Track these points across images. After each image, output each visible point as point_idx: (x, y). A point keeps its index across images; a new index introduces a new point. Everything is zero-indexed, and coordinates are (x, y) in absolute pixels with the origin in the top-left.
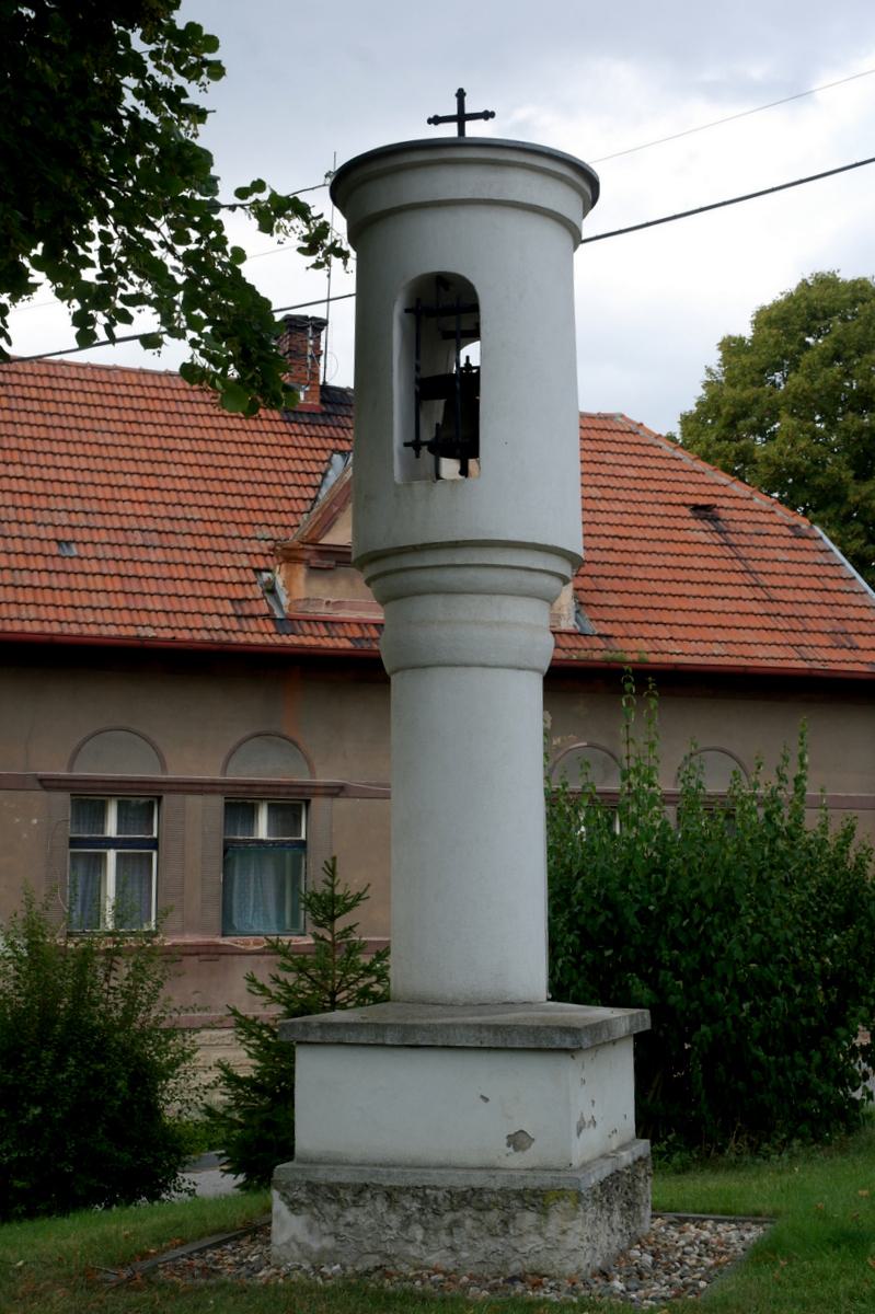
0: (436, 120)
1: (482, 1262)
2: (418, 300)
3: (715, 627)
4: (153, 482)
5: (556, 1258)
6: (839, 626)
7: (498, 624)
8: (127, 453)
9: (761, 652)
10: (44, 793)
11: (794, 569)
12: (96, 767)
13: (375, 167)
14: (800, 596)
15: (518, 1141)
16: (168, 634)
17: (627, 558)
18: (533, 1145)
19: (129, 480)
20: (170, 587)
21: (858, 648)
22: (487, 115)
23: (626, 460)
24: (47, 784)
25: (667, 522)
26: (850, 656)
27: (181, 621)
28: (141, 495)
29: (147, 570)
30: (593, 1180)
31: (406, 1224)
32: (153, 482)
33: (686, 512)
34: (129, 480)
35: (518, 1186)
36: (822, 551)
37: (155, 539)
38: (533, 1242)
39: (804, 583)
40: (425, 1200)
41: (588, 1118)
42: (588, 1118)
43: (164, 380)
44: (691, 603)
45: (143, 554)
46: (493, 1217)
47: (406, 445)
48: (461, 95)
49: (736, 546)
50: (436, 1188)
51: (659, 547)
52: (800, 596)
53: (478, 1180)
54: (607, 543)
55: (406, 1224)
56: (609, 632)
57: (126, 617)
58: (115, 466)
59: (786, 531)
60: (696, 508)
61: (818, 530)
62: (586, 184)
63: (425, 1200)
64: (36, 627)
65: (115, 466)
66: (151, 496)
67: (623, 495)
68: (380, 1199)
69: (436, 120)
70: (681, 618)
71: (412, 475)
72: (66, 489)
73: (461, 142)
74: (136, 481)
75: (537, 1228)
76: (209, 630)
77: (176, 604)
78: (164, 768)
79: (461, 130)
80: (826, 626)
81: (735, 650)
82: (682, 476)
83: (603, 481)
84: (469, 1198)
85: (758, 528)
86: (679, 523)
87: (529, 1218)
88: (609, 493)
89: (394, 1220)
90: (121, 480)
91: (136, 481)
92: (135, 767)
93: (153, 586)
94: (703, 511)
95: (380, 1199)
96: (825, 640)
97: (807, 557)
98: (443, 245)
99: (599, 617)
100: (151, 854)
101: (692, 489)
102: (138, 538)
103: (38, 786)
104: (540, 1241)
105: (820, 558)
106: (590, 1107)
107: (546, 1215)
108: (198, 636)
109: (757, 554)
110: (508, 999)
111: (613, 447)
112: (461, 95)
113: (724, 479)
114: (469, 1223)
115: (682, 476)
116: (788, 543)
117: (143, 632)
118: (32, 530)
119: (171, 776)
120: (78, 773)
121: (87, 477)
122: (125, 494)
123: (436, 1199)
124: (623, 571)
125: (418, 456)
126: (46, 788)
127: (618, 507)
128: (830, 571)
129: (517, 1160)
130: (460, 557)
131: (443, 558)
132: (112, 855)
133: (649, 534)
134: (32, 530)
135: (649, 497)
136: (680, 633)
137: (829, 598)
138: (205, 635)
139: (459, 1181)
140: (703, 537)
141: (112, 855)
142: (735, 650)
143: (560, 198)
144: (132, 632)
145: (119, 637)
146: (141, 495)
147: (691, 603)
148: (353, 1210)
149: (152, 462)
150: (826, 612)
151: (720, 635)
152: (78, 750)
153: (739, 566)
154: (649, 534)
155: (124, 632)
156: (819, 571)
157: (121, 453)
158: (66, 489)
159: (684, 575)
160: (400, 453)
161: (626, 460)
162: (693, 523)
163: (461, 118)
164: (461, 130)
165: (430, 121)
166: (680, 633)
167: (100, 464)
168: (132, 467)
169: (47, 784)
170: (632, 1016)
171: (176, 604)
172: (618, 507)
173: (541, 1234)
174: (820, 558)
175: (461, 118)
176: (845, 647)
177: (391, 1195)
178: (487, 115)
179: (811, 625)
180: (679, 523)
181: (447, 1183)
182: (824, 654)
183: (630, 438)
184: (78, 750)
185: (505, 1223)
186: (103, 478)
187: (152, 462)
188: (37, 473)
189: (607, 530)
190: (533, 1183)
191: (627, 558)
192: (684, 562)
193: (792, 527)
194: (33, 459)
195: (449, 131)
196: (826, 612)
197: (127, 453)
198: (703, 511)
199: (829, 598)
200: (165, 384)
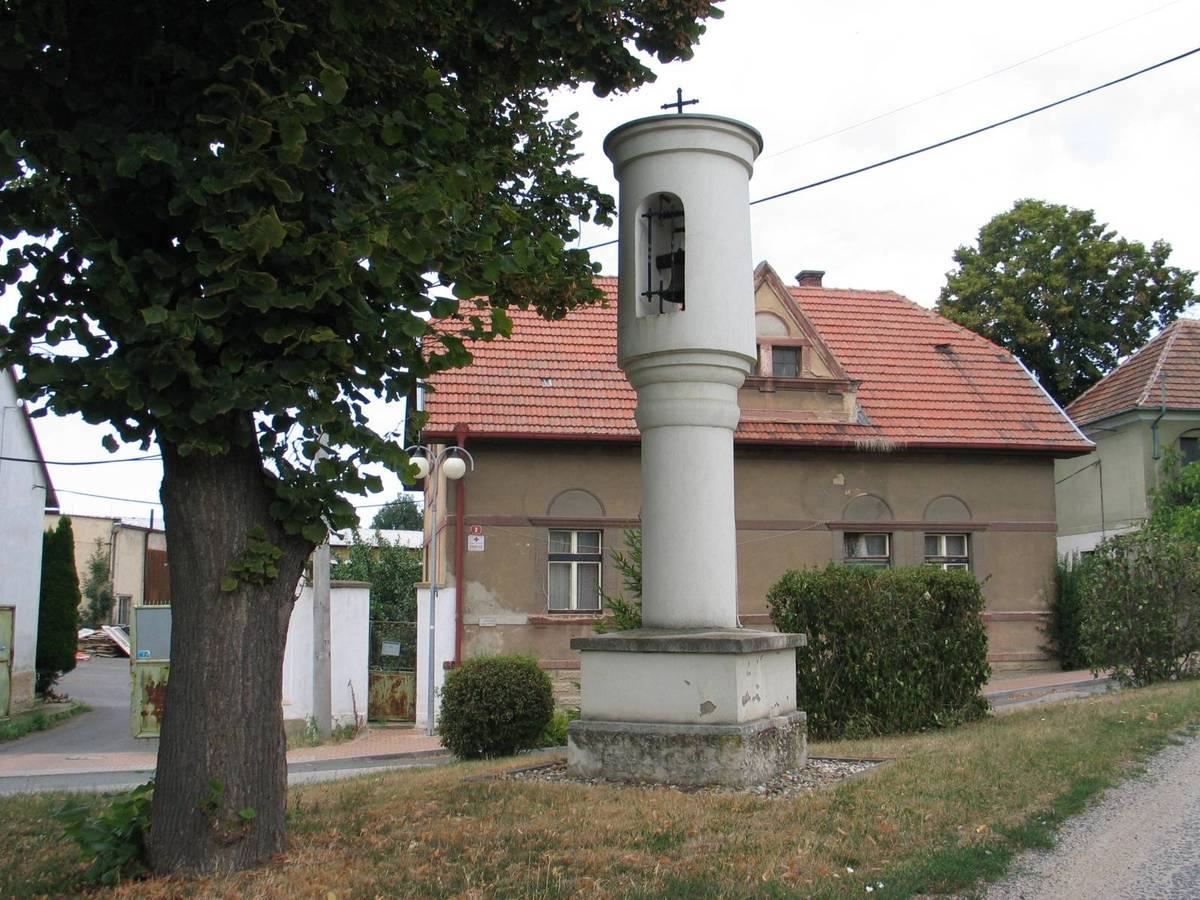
0: (665, 107)
1: (685, 777)
2: (650, 210)
3: (948, 419)
4: (599, 341)
5: (727, 775)
6: (1027, 417)
7: (701, 399)
8: (585, 325)
9: (976, 434)
10: (533, 528)
11: (1000, 382)
12: (564, 512)
13: (622, 135)
14: (1003, 399)
15: (707, 707)
16: (604, 431)
17: (893, 378)
18: (716, 710)
19: (585, 341)
20: (607, 404)
21: (1038, 430)
22: (694, 102)
23: (893, 318)
24: (534, 522)
25: (919, 356)
26: (1034, 435)
27: (612, 423)
28: (592, 349)
29: (593, 394)
30: (756, 727)
31: (642, 754)
32: (599, 341)
33: (932, 349)
34: (585, 341)
35: (704, 733)
36: (1018, 371)
37: (598, 375)
38: (713, 765)
39: (1006, 391)
40: (652, 741)
41: (752, 695)
42: (752, 695)
43: (609, 281)
44: (932, 405)
45: (591, 384)
46: (690, 751)
47: (643, 294)
48: (679, 91)
49: (963, 369)
50: (659, 734)
51: (913, 371)
52: (1003, 399)
53: (682, 729)
54: (881, 369)
55: (642, 754)
56: (880, 424)
57: (579, 422)
58: (578, 333)
59: (995, 359)
60: (938, 346)
61: (1017, 359)
62: (756, 140)
63: (652, 741)
64: (526, 429)
65: (578, 333)
66: (597, 350)
67: (891, 340)
68: (627, 741)
69: (665, 107)
70: (926, 414)
71: (648, 311)
72: (547, 348)
73: (681, 117)
74: (589, 341)
75: (716, 758)
76: (629, 428)
77: (609, 414)
78: (604, 513)
79: (680, 111)
80: (1018, 417)
81: (961, 433)
82: (930, 327)
83: (880, 332)
84: (682, 740)
85: (977, 358)
86: (927, 356)
87: (711, 752)
88: (884, 339)
89: (635, 752)
90: (580, 341)
91: (589, 341)
92: (588, 511)
93: (596, 403)
94: (942, 348)
95: (627, 741)
96: (1018, 426)
97: (1011, 375)
98: (663, 177)
99: (874, 414)
100: (598, 565)
101: (936, 335)
102: (588, 375)
103: (529, 523)
104: (717, 765)
105: (1017, 375)
106: (767, 688)
107: (721, 750)
108: (622, 432)
109: (975, 373)
110: (708, 625)
111: (887, 311)
112: (679, 91)
113: (956, 327)
114: (676, 755)
115: (930, 327)
116: (996, 366)
117: (589, 431)
118: (527, 373)
119: (609, 516)
120: (553, 516)
121: (560, 340)
122: (582, 349)
123: (658, 740)
124: (890, 387)
125: (650, 300)
126: (534, 525)
127: (889, 347)
128: (1023, 383)
129: (706, 718)
130: (674, 359)
131: (666, 360)
132: (574, 565)
133: (907, 363)
134: (527, 373)
135: (910, 341)
136: (925, 423)
137: (1022, 400)
138: (626, 432)
139: (673, 730)
140: (942, 364)
141: (574, 565)
142: (961, 433)
143: (743, 150)
144: (582, 430)
145: (574, 434)
146: (592, 349)
147: (932, 405)
148: (612, 747)
149: (530, 319)
150: (1020, 408)
151: (951, 424)
152: (553, 501)
153: (964, 381)
154: (907, 363)
155: (577, 431)
156: (1016, 383)
157: (581, 325)
158: (547, 348)
159: (929, 388)
160: (641, 300)
161: (893, 318)
162: (936, 356)
163: (680, 104)
164: (680, 111)
165: (662, 107)
166: (925, 423)
167: (568, 332)
168: (587, 333)
169: (534, 522)
170: (790, 638)
171: (609, 414)
172: (889, 347)
173: (718, 761)
174: (1017, 375)
175: (680, 104)
176: (1030, 430)
177: (633, 738)
178: (694, 102)
179: (1009, 417)
180: (927, 356)
181: (664, 732)
182: (1016, 434)
183: (900, 305)
184: (553, 501)
185: (698, 754)
186: (570, 340)
187: (530, 319)
188: (530, 339)
189: (881, 362)
190: (713, 730)
191: (893, 378)
192: (931, 380)
193: (999, 356)
194: (529, 330)
195: (674, 111)
196: (1020, 408)
197: (585, 325)
198: (942, 348)
199: (1022, 400)
200: (609, 283)
